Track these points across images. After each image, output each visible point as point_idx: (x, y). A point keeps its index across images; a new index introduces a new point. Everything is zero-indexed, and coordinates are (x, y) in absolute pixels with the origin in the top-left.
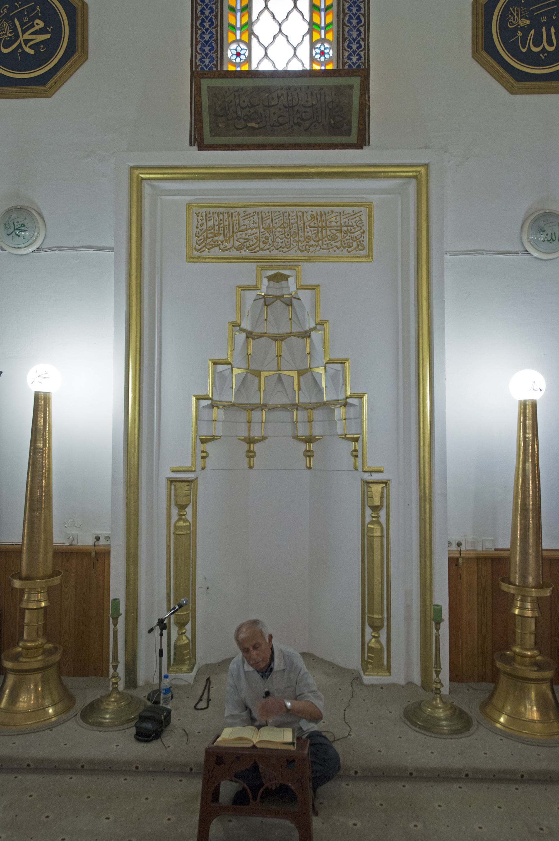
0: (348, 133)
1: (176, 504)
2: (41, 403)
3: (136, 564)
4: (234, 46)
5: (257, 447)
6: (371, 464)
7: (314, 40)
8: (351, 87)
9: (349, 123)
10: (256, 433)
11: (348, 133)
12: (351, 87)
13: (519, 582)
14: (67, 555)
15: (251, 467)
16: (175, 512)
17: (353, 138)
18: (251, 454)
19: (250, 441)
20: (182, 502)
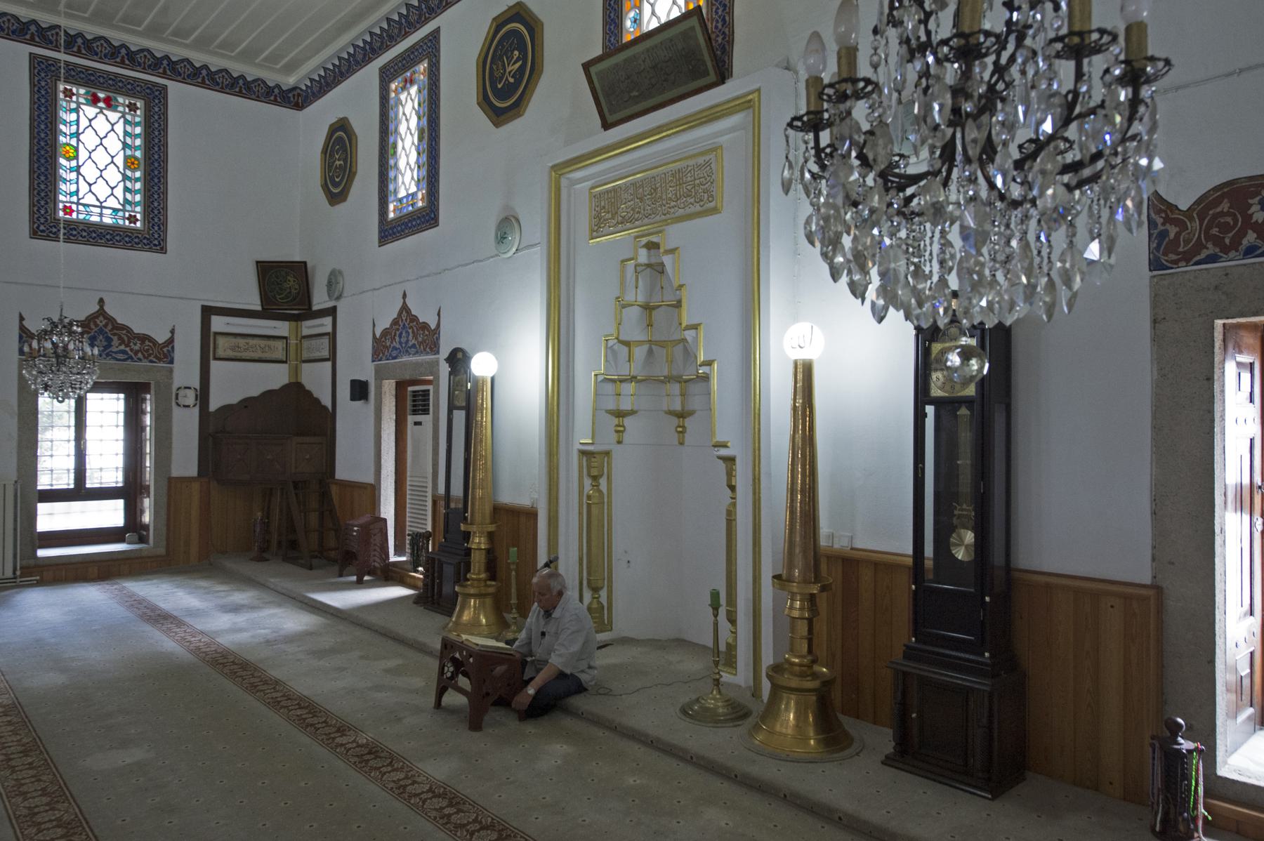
0: (706, 73)
1: (589, 475)
2: (805, 375)
3: (556, 527)
4: (138, 119)
5: (627, 421)
6: (719, 438)
7: (177, 91)
8: (693, 28)
9: (704, 63)
10: (626, 405)
11: (706, 73)
12: (693, 28)
13: (352, 575)
14: (499, 511)
15: (681, 444)
16: (588, 482)
17: (712, 77)
18: (682, 431)
19: (620, 414)
20: (595, 472)
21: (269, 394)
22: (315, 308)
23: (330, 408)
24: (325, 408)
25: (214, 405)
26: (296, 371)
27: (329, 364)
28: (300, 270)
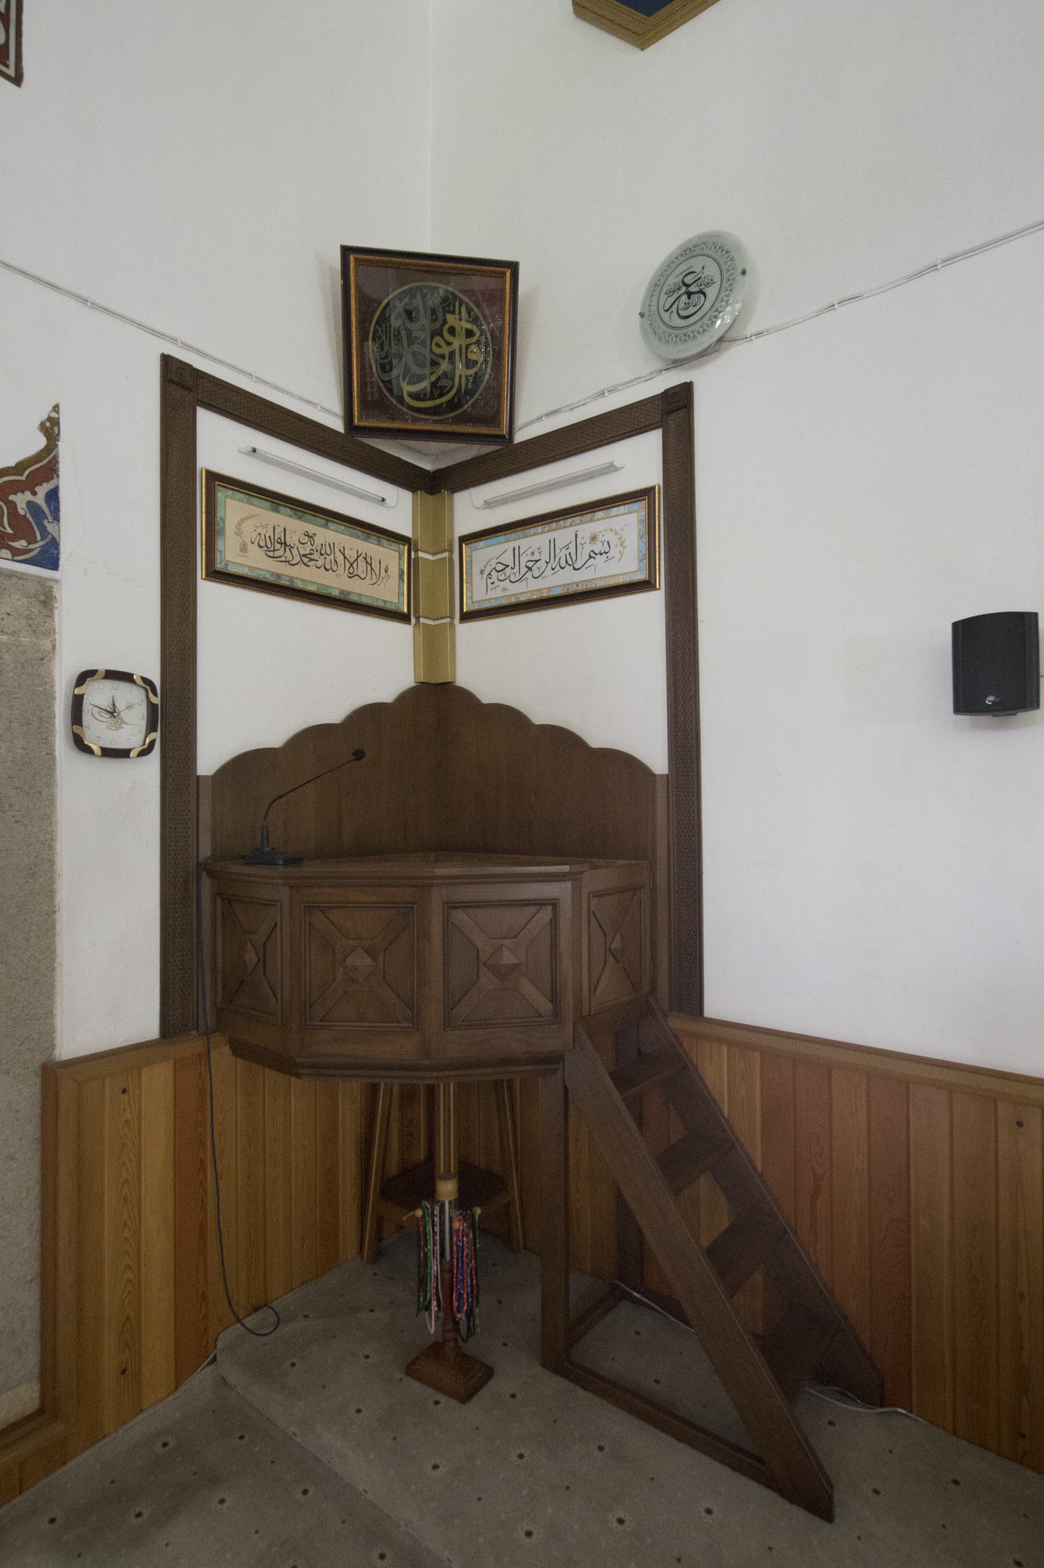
21: (368, 716)
22: (520, 436)
23: (654, 754)
24: (623, 765)
25: (213, 751)
26: (434, 648)
27: (652, 605)
28: (486, 289)
